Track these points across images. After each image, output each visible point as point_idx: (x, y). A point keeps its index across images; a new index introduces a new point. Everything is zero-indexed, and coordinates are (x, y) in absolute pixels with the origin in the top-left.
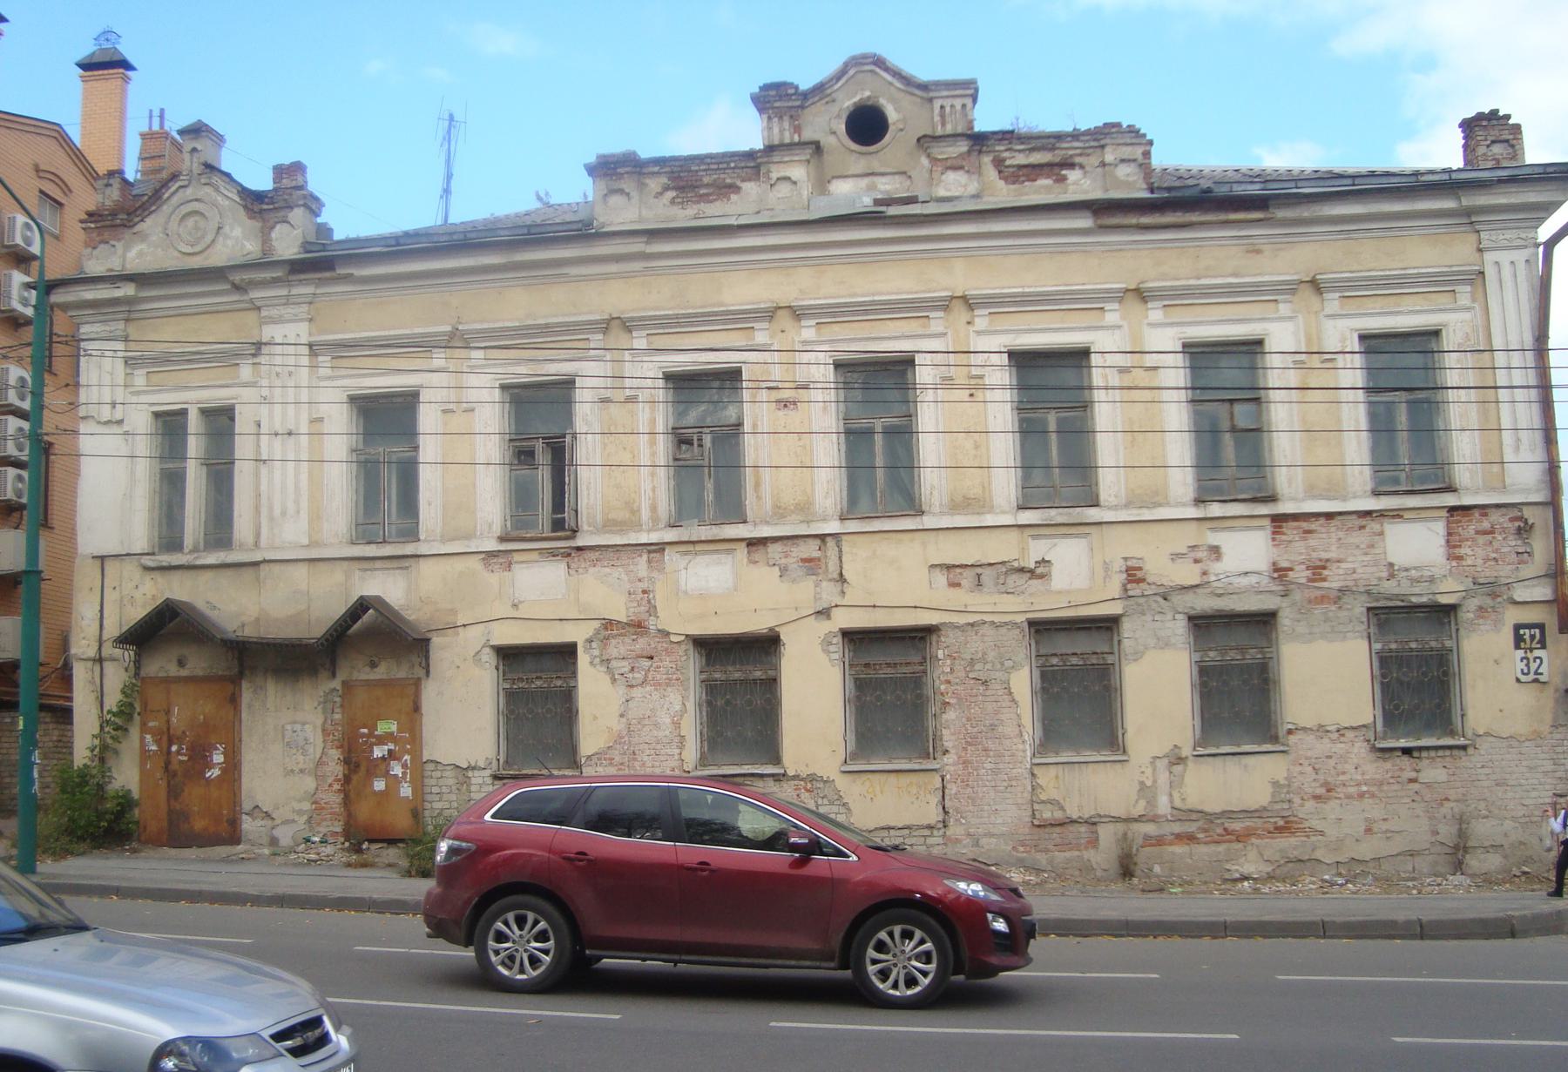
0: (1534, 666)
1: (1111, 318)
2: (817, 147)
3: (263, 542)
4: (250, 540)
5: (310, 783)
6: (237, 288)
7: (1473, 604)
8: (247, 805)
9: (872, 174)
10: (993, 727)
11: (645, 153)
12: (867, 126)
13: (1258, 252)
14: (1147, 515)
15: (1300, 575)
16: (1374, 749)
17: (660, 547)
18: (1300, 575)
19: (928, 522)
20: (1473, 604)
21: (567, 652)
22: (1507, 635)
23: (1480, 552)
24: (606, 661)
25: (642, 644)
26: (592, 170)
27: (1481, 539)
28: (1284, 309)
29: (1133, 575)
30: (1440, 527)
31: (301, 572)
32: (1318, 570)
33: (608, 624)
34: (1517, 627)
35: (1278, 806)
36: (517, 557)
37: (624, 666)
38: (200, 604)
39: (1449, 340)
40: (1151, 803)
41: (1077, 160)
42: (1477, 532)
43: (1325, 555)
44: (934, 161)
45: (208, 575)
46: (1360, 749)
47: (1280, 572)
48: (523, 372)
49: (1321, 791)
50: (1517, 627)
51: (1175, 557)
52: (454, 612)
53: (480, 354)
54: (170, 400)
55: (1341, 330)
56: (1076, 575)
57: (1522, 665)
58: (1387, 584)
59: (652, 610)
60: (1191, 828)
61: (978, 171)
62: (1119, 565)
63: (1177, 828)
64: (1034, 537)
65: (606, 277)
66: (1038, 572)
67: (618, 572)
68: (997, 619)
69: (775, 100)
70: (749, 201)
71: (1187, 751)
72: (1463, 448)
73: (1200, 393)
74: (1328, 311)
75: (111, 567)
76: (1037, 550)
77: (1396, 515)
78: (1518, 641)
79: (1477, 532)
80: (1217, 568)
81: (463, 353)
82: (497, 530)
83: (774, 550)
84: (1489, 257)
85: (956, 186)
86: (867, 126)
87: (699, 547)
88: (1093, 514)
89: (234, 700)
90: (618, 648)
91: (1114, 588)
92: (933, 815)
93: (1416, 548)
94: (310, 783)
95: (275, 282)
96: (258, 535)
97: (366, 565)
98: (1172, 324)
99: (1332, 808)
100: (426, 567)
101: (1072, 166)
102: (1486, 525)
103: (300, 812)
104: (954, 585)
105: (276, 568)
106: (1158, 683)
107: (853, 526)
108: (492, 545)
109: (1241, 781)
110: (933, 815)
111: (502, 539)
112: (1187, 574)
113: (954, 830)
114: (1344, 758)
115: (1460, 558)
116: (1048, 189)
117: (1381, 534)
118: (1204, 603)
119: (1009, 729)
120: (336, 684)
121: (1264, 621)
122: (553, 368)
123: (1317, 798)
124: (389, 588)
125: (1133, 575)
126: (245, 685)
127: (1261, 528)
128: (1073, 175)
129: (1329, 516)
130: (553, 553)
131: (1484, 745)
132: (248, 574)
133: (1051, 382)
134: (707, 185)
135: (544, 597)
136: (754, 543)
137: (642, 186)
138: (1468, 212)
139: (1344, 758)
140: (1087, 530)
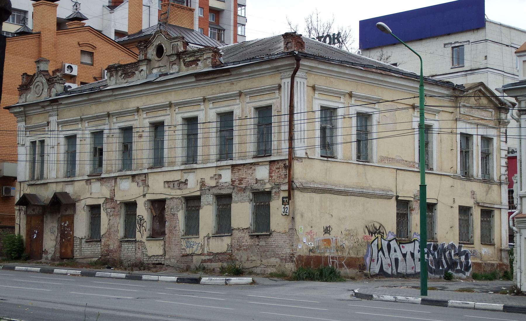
0: (286, 210)
2: (149, 61)
3: (45, 176)
6: (43, 107)
9: (160, 67)
10: (175, 227)
13: (233, 84)
14: (205, 166)
15: (237, 183)
16: (250, 235)
17: (115, 178)
18: (237, 183)
19: (164, 169)
20: (274, 191)
23: (276, 175)
25: (112, 205)
27: (277, 171)
28: (238, 101)
29: (203, 184)
30: (268, 167)
31: (54, 185)
32: (241, 180)
33: (106, 199)
34: (283, 198)
35: (229, 252)
36: (92, 181)
38: (37, 195)
40: (203, 250)
41: (200, 58)
42: (276, 169)
43: (242, 177)
45: (39, 187)
46: (247, 236)
47: (233, 181)
49: (238, 247)
50: (283, 198)
52: (80, 196)
54: (33, 139)
57: (283, 210)
58: (255, 185)
60: (211, 257)
61: (179, 65)
62: (199, 180)
63: (208, 257)
64: (185, 173)
65: (109, 101)
67: (109, 185)
68: (176, 197)
71: (210, 235)
73: (323, 119)
74: (247, 101)
75: (22, 185)
76: (186, 176)
77: (257, 164)
78: (283, 202)
79: (276, 169)
80: (221, 181)
82: (252, 154)
84: (283, 81)
87: (123, 177)
88: (195, 166)
89: (42, 221)
90: (108, 206)
91: (198, 188)
92: (161, 252)
93: (262, 173)
95: (48, 106)
97: (66, 183)
98: (214, 108)
99: (241, 253)
102: (278, 166)
103: (52, 251)
105: (50, 184)
108: (86, 178)
110: (161, 252)
111: (255, 157)
112: (213, 183)
113: (167, 257)
114: (243, 238)
115: (272, 177)
116: (193, 69)
117: (255, 170)
118: (216, 191)
120: (59, 216)
122: (100, 128)
123: (237, 249)
124: (69, 189)
125: (203, 184)
127: (228, 169)
128: (199, 63)
129: (244, 165)
131: (274, 234)
134: (130, 73)
136: (133, 176)
137: (117, 73)
138: (277, 67)
139: (243, 238)
140: (194, 170)
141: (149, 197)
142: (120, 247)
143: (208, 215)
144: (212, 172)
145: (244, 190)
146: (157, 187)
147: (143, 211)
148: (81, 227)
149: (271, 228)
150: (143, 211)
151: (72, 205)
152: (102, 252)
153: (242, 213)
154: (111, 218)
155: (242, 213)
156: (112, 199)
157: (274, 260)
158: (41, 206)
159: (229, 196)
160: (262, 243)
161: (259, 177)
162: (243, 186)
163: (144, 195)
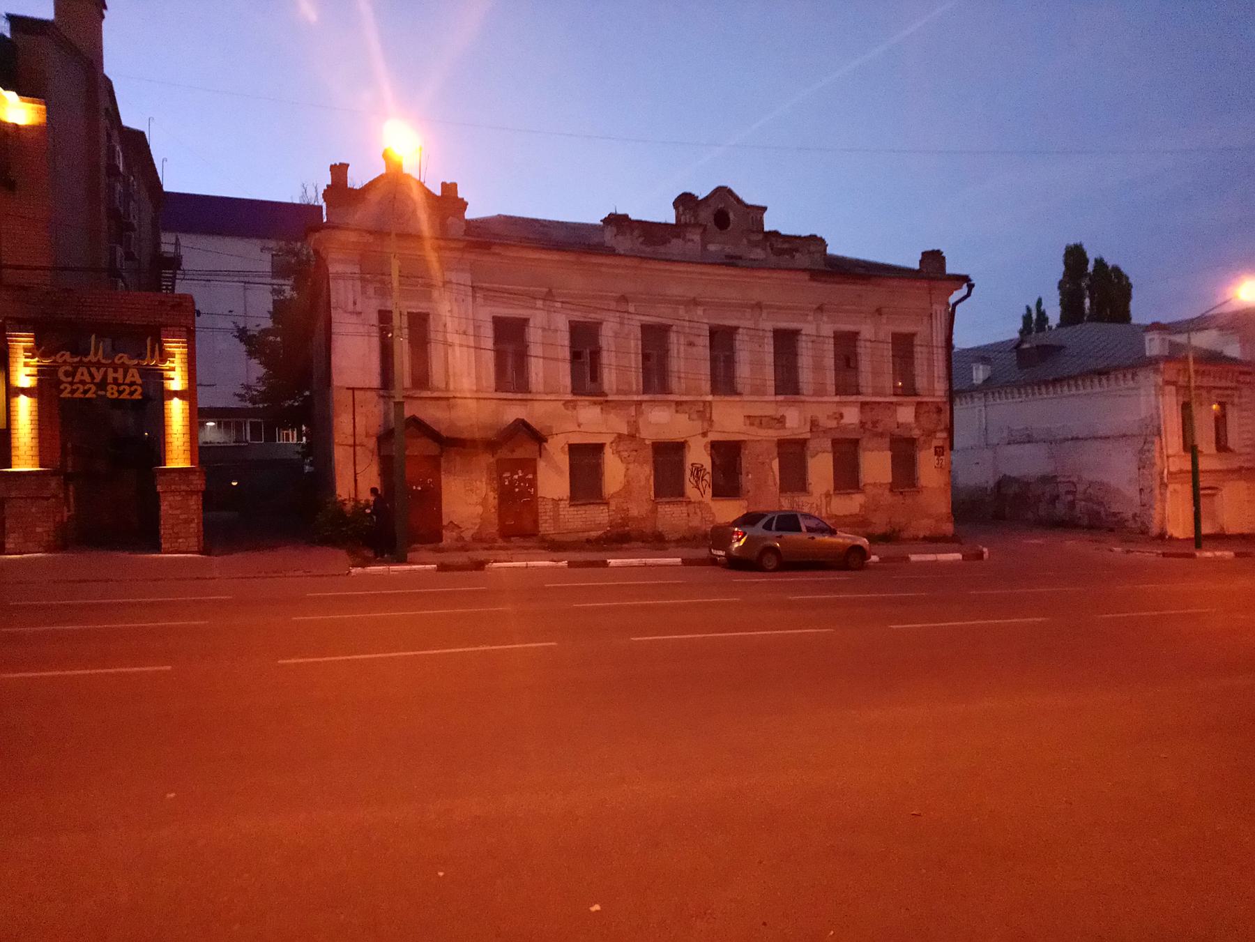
1: (810, 318)
3: (452, 387)
4: (443, 386)
5: (480, 509)
7: (923, 438)
8: (445, 523)
11: (633, 217)
12: (721, 220)
14: (820, 399)
15: (869, 425)
17: (640, 403)
18: (869, 425)
21: (599, 448)
22: (933, 450)
24: (618, 452)
26: (449, 189)
29: (814, 424)
32: (875, 424)
37: (625, 454)
39: (862, 337)
44: (749, 241)
47: (862, 424)
48: (578, 316)
51: (828, 417)
53: (558, 305)
55: (827, 329)
56: (795, 421)
59: (637, 430)
66: (781, 421)
69: (685, 202)
70: (676, 246)
72: (921, 383)
76: (783, 411)
77: (900, 404)
78: (936, 453)
81: (551, 304)
83: (685, 407)
85: (758, 253)
86: (721, 220)
89: (438, 468)
93: (906, 415)
94: (480, 509)
96: (447, 384)
100: (536, 404)
101: (797, 251)
104: (752, 424)
106: (821, 468)
107: (646, 397)
109: (851, 505)
112: (833, 424)
118: (838, 436)
119: (770, 482)
121: (856, 442)
125: (814, 424)
126: (443, 460)
128: (797, 255)
130: (595, 403)
132: (444, 403)
133: (786, 341)
135: (591, 422)
136: (678, 403)
141: (713, 436)
142: (654, 511)
143: (821, 468)
144: (833, 409)
145: (882, 435)
146: (730, 420)
147: (698, 455)
148: (553, 481)
149: (861, 476)
150: (698, 455)
151: (538, 438)
152: (611, 522)
153: (876, 465)
154: (631, 466)
155: (876, 465)
156: (632, 437)
157: (925, 522)
158: (379, 446)
159: (856, 442)
160: (909, 501)
161: (901, 420)
162: (880, 430)
163: (704, 434)
